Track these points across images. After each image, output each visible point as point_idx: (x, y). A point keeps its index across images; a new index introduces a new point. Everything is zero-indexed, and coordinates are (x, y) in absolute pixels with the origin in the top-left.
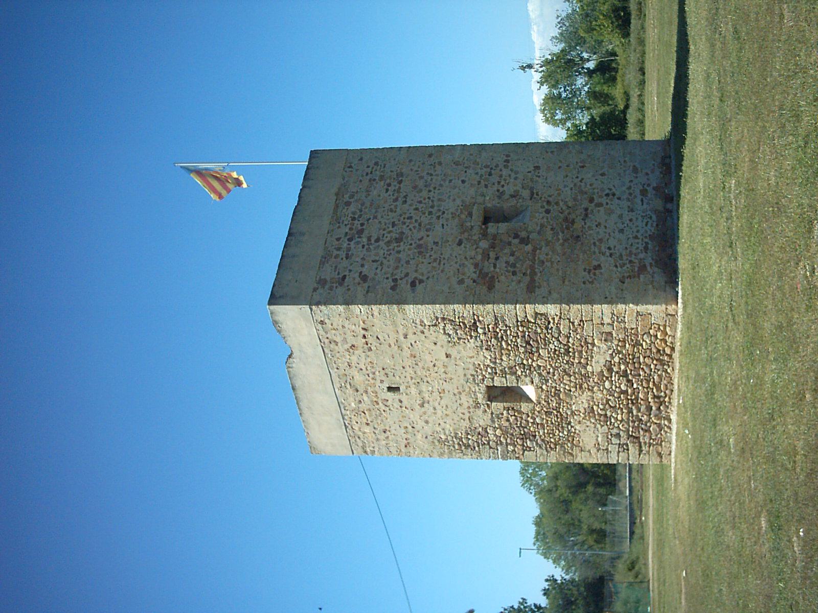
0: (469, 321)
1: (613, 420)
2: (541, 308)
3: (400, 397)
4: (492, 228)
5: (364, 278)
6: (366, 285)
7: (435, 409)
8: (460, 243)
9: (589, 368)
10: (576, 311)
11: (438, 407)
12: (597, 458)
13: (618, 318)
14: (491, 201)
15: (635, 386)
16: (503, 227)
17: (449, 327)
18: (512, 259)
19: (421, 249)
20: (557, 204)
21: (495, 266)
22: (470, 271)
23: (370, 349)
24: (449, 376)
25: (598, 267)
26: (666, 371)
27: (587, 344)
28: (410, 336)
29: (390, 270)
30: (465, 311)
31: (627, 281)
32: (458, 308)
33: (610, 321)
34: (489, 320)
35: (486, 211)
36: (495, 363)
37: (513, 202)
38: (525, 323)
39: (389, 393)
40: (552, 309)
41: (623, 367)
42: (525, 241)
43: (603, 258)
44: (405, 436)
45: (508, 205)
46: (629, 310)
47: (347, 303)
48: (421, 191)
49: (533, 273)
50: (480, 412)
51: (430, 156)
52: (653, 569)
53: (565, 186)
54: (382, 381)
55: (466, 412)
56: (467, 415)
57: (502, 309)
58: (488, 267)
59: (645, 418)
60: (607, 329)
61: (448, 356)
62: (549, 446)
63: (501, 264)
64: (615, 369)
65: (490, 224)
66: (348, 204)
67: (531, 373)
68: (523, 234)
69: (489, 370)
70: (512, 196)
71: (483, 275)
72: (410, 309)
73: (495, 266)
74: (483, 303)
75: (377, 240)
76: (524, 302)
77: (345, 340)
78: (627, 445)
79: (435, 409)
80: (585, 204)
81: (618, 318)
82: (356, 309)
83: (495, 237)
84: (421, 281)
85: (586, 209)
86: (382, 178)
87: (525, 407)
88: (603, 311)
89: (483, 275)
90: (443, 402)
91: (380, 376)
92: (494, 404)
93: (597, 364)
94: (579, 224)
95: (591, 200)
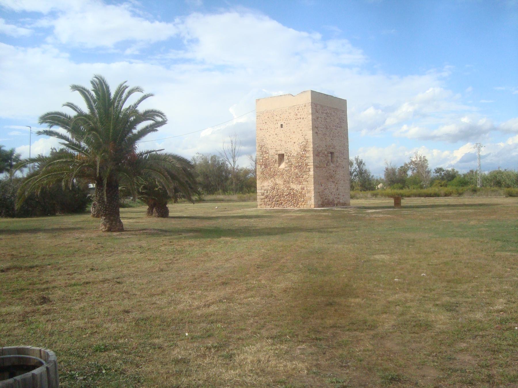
0: (307, 149)
1: (273, 191)
2: (312, 170)
3: (279, 128)
4: (330, 155)
5: (318, 118)
6: (316, 119)
7: (275, 138)
8: (326, 146)
9: (291, 184)
10: (312, 180)
11: (275, 139)
12: (259, 186)
13: (309, 192)
14: (336, 154)
15: (285, 197)
16: (330, 158)
17: (305, 143)
18: (323, 161)
19: (325, 134)
20: (335, 174)
21: (321, 156)
22: (320, 149)
23: (296, 120)
24: (287, 143)
25: (322, 186)
26: (291, 205)
27: (300, 183)
28: (301, 132)
29: (320, 126)
30: (310, 148)
31: (319, 194)
32: (312, 146)
33: (308, 189)
34: (307, 155)
35: (333, 153)
36: (292, 156)
37: (336, 161)
38: (307, 165)
39: (280, 125)
40: (312, 173)
41: (292, 193)
42: (327, 165)
43: (324, 187)
44: (264, 129)
45: (335, 159)
46: (312, 194)
47: (312, 114)
48: (338, 134)
49: (320, 167)
50: (274, 151)
51: (346, 136)
52: (420, 195)
53: (339, 176)
54: (284, 123)
55: (274, 147)
56: (273, 148)
57: (311, 158)
58: (321, 154)
59: (274, 200)
60: (305, 189)
61: (294, 143)
62: (262, 173)
63: (322, 158)
64: (291, 191)
65: (330, 154)
66: (334, 112)
67: (289, 167)
68: (328, 164)
69: (289, 155)
70: (337, 160)
71: (319, 153)
72: (311, 132)
73: (321, 156)
74: (313, 153)
75: (326, 121)
76: (313, 165)
77: (299, 112)
78: (264, 195)
79: (275, 138)
80: (336, 182)
81: (309, 192)
82: (310, 116)
83: (328, 156)
84: (317, 135)
85: (334, 182)
86: (340, 122)
87: (276, 165)
88: (311, 187)
89: (319, 153)
90: (277, 141)
91: (286, 122)
92: (278, 156)
93: (293, 186)
94: (331, 180)
95: (336, 183)
